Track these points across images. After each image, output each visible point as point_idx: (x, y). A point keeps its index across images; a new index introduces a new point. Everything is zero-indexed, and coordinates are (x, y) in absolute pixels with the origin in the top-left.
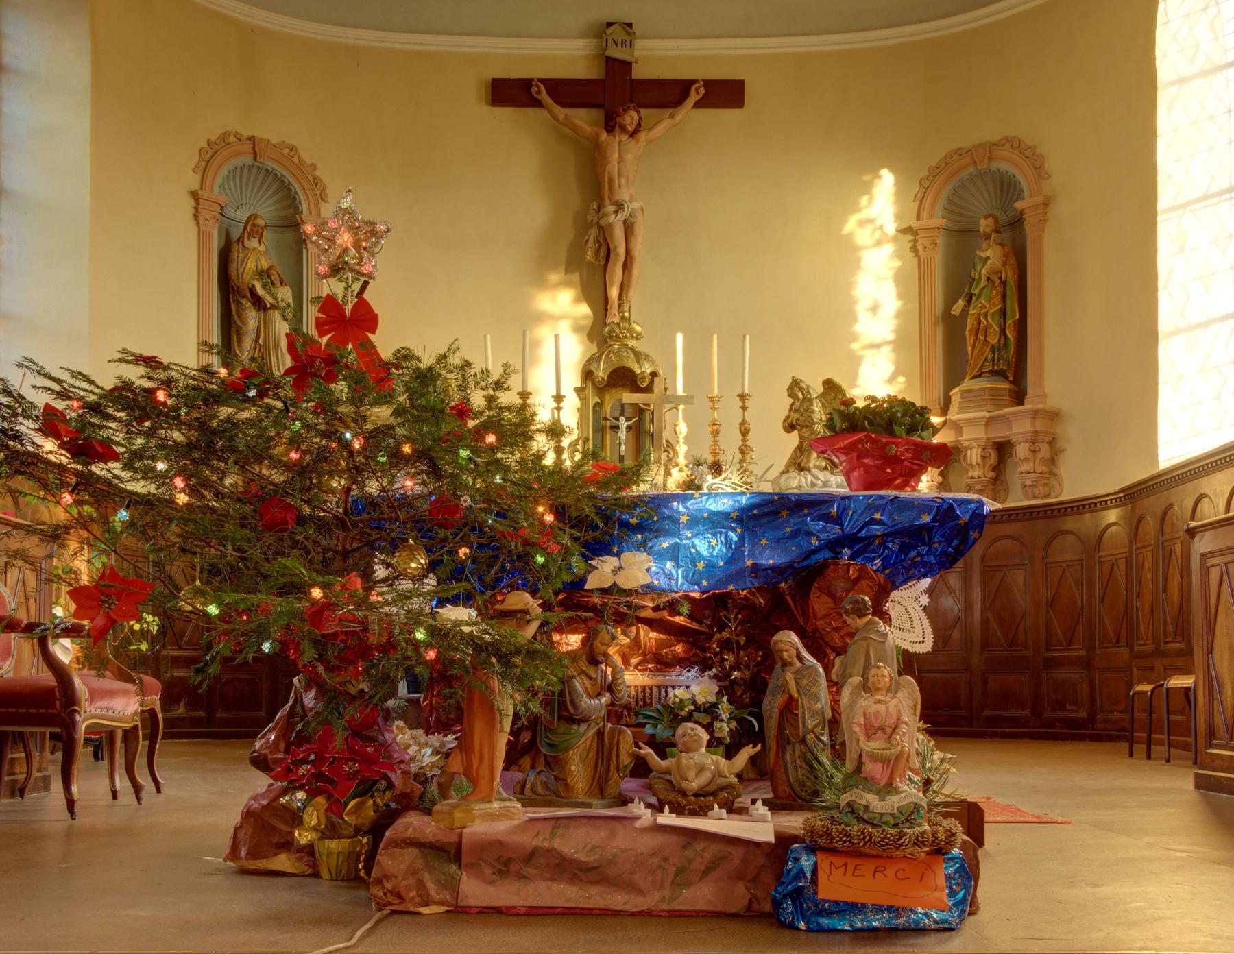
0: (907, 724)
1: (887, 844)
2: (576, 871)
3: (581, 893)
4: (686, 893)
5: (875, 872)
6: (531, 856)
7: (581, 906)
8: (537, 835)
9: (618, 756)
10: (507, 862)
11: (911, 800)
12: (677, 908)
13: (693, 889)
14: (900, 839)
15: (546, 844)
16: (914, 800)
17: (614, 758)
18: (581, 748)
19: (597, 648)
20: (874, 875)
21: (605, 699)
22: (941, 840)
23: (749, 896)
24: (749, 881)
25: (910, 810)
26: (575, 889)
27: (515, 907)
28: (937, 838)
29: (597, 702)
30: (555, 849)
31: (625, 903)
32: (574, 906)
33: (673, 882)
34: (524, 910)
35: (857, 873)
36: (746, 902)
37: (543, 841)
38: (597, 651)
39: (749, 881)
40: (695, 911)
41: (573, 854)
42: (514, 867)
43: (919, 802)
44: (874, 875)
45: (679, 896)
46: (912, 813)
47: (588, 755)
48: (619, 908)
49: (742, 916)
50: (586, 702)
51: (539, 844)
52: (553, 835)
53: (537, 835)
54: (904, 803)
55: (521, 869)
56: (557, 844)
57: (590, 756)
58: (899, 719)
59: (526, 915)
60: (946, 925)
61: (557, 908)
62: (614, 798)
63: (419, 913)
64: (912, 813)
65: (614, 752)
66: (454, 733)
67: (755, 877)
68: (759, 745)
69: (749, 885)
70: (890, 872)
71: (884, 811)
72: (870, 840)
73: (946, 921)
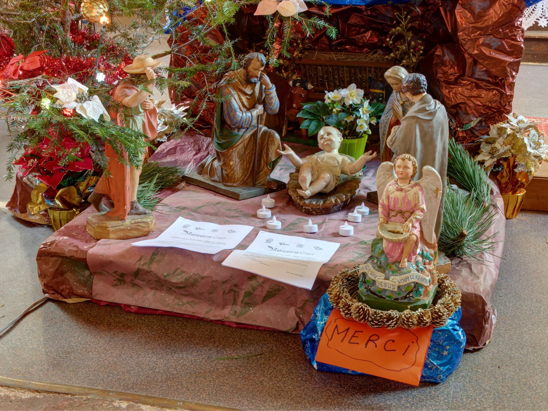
0: (422, 210)
1: (376, 324)
2: (171, 287)
3: (177, 301)
4: (252, 311)
5: (369, 340)
6: (137, 273)
7: (175, 311)
8: (140, 260)
9: (267, 154)
10: (122, 275)
11: (411, 281)
12: (243, 322)
13: (257, 308)
14: (388, 321)
15: (146, 268)
16: (415, 280)
17: (264, 156)
18: (240, 147)
19: (251, 72)
20: (366, 344)
21: (260, 109)
22: (427, 323)
23: (297, 320)
24: (299, 308)
25: (410, 289)
26: (172, 297)
27: (129, 306)
28: (422, 321)
29: (249, 114)
30: (151, 271)
31: (207, 312)
32: (170, 310)
33: (242, 301)
34: (134, 309)
35: (354, 340)
36: (294, 325)
37: (143, 265)
38: (251, 74)
39: (299, 308)
40: (256, 326)
41: (165, 276)
42: (128, 279)
43: (419, 282)
44: (366, 344)
45: (247, 312)
46: (411, 291)
47: (245, 152)
48: (202, 316)
49: (291, 334)
50: (242, 115)
51: (141, 267)
52: (152, 261)
53: (140, 260)
54: (405, 283)
55: (132, 280)
56: (154, 268)
57: (247, 153)
58: (415, 205)
59: (136, 313)
60: (431, 380)
61: (158, 310)
62: (264, 185)
63: (65, 302)
64: (411, 291)
65: (265, 150)
66: (185, 105)
67: (302, 307)
68: (375, 153)
69: (299, 310)
70: (380, 342)
71: (387, 288)
72: (364, 318)
73: (432, 378)
